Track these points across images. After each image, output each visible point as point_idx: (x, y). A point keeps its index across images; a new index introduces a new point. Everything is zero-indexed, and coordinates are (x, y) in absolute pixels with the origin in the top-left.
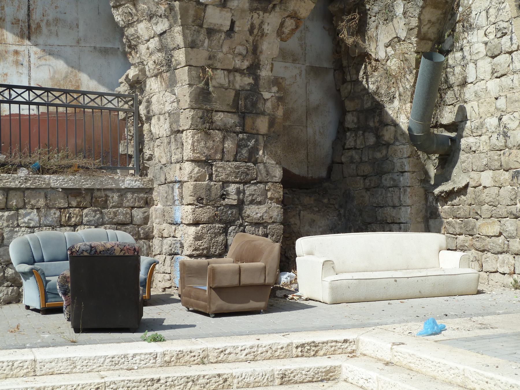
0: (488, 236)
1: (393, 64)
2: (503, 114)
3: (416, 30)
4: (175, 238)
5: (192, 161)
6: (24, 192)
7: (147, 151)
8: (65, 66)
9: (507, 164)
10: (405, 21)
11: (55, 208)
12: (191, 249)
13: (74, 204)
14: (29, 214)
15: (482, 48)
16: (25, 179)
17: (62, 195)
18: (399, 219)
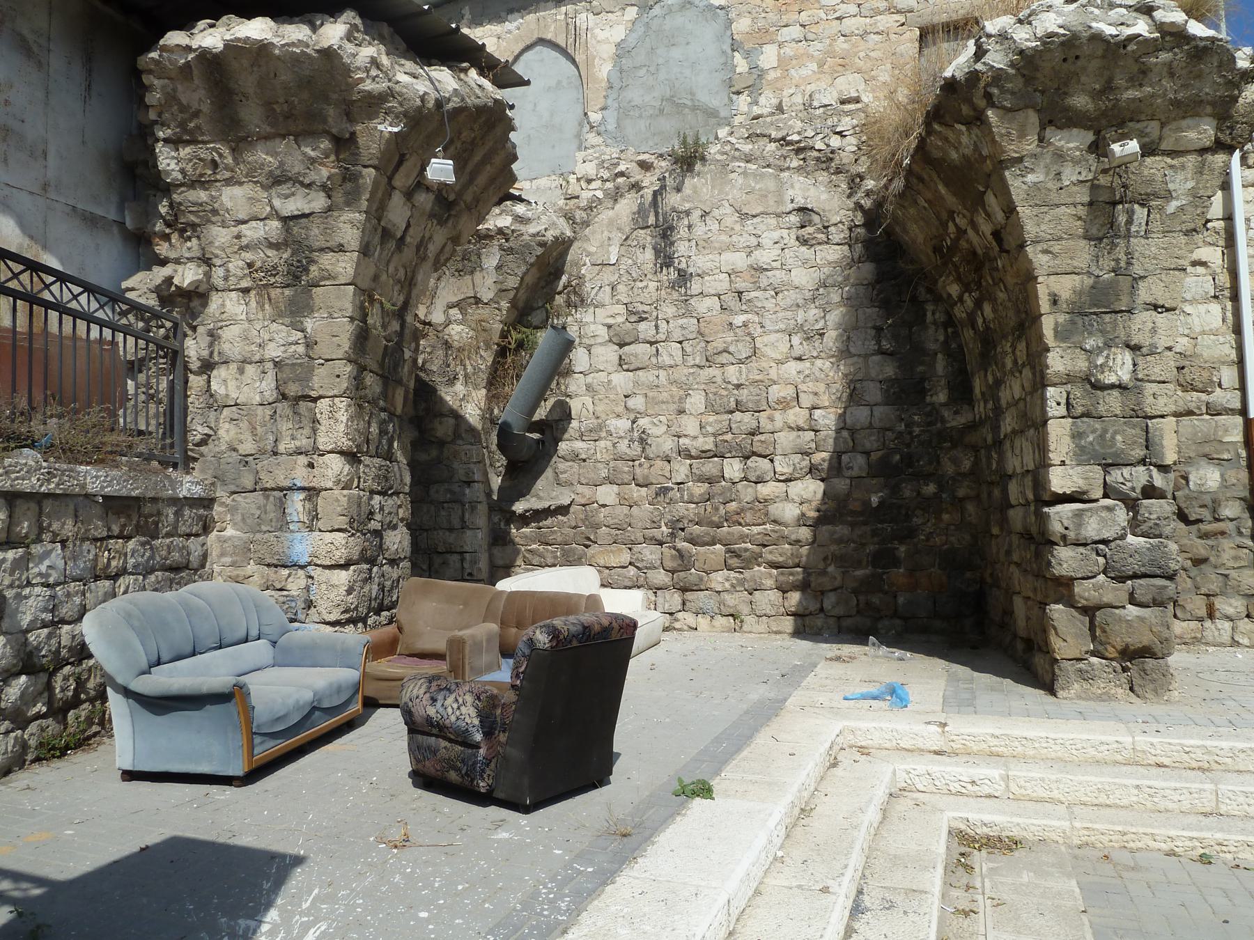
0: (607, 568)
1: (458, 332)
2: (638, 416)
4: (285, 593)
5: (342, 453)
6: (40, 504)
7: (200, 428)
8: (18, 231)
9: (646, 477)
11: (88, 539)
13: (116, 529)
14: (47, 554)
15: (603, 333)
16: (48, 473)
17: (97, 510)
18: (462, 547)
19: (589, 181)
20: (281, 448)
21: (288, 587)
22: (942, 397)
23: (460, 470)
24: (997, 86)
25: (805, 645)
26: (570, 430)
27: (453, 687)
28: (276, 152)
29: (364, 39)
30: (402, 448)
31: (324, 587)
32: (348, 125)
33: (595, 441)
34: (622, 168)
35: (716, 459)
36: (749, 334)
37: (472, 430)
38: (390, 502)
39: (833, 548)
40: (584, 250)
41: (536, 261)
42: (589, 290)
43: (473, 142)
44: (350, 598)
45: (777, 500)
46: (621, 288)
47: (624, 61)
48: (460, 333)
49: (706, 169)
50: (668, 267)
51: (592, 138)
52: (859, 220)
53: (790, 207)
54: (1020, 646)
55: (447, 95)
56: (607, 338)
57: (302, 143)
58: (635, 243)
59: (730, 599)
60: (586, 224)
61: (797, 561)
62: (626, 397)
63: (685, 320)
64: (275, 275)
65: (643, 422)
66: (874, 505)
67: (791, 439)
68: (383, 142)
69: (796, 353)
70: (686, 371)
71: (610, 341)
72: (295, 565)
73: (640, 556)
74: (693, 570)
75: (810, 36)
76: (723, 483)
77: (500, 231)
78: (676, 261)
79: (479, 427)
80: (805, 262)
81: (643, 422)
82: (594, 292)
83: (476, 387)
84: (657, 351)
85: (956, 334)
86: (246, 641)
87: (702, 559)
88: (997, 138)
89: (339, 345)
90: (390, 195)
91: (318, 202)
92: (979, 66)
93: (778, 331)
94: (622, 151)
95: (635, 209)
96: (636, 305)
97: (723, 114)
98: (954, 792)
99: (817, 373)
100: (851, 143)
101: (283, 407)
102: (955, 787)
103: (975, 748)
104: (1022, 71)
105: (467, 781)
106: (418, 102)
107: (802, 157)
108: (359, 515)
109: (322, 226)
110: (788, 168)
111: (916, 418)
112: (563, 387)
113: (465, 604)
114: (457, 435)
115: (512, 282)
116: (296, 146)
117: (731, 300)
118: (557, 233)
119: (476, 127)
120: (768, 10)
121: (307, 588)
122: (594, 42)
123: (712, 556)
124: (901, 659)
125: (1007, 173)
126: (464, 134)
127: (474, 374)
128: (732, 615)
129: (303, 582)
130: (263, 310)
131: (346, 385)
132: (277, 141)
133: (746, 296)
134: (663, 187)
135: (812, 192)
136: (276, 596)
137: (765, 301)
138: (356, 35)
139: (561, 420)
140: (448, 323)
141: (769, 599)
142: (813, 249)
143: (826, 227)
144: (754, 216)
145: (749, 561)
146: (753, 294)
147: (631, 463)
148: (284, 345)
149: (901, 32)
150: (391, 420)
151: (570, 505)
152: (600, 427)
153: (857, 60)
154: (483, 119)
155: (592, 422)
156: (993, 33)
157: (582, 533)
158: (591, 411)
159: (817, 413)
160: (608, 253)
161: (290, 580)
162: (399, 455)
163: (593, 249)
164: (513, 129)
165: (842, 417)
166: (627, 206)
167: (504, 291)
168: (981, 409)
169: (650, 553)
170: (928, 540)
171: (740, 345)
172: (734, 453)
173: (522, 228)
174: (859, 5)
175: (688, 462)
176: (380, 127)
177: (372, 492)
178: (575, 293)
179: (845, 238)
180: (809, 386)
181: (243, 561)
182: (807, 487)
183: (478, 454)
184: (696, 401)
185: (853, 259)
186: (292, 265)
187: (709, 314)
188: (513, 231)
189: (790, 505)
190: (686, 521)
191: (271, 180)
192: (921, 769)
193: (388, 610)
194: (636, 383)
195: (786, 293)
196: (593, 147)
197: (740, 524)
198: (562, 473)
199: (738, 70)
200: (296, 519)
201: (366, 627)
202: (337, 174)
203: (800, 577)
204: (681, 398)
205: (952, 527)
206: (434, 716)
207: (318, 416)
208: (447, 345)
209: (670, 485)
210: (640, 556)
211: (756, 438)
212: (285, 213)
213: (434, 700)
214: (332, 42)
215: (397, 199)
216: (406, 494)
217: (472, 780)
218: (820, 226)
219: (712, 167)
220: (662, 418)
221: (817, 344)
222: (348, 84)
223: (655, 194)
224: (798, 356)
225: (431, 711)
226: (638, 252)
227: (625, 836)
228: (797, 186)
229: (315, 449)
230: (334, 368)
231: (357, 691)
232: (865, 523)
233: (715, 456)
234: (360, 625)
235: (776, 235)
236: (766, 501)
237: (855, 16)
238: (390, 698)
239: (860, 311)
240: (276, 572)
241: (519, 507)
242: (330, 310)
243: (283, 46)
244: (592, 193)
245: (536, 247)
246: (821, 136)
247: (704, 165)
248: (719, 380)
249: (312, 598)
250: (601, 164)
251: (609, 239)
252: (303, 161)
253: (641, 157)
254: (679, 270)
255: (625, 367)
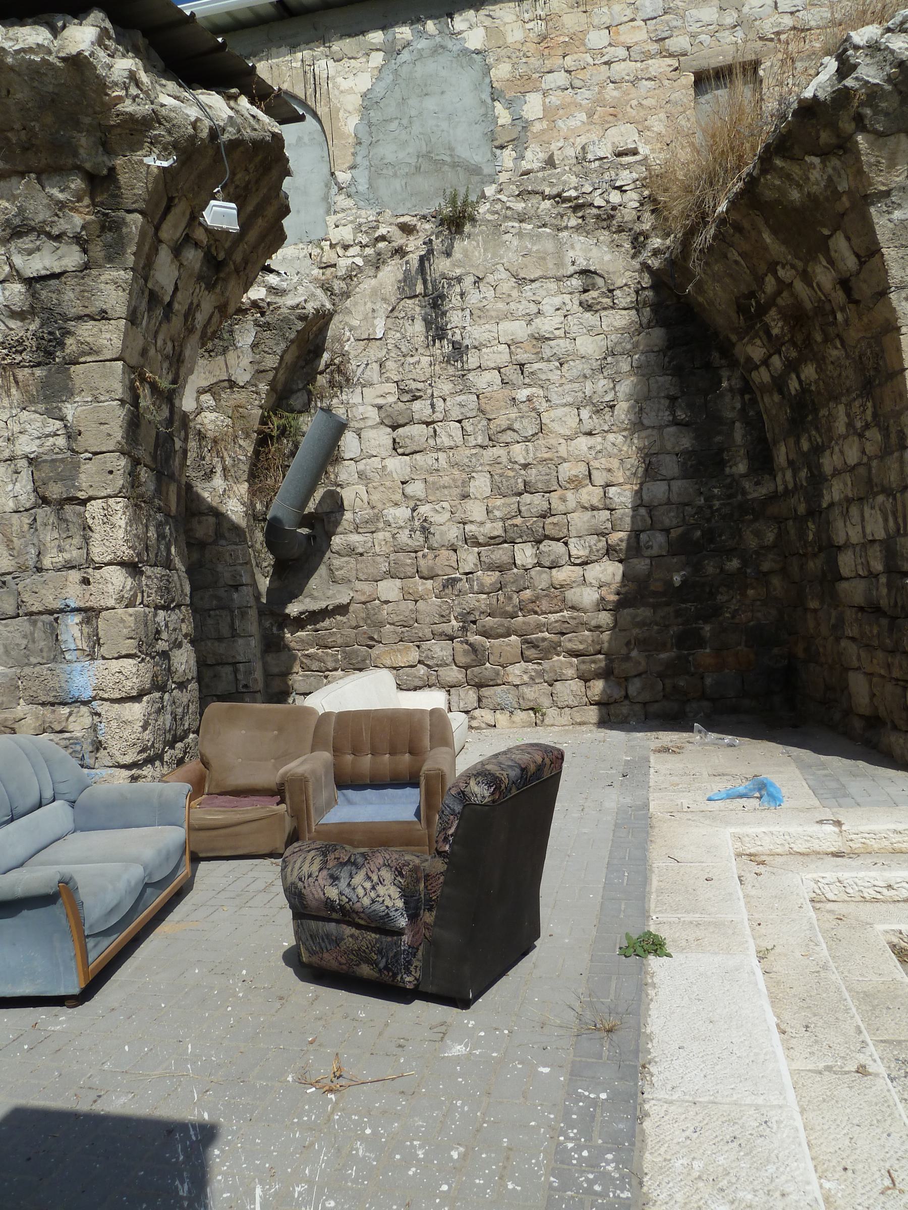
2: (418, 503)
3: (271, 375)
4: (67, 735)
5: (122, 564)
9: (431, 569)
10: (254, 357)
12: (134, 750)
15: (373, 415)
19: (346, 247)
20: (47, 562)
21: (70, 728)
22: (742, 468)
23: (226, 576)
24: (871, 106)
25: (616, 736)
26: (344, 523)
27: (360, 860)
28: (13, 195)
29: (116, 49)
30: (179, 553)
31: (114, 724)
32: (105, 159)
33: (372, 532)
34: (382, 231)
35: (506, 545)
36: (534, 409)
37: (235, 528)
38: (174, 617)
39: (636, 631)
40: (346, 323)
41: (297, 336)
42: (355, 368)
43: (246, 187)
44: (147, 735)
45: (574, 585)
46: (390, 364)
47: (372, 113)
48: (215, 421)
49: (477, 230)
50: (441, 339)
51: (342, 201)
52: (646, 281)
53: (571, 269)
54: (858, 724)
55: (222, 124)
56: (378, 420)
57: (46, 183)
58: (403, 314)
59: (530, 693)
60: (346, 295)
61: (598, 647)
62: (403, 483)
63: (463, 397)
64: (21, 352)
65: (424, 509)
66: (677, 585)
67: (585, 519)
68: (151, 179)
69: (587, 427)
70: (468, 452)
71: (382, 423)
72: (76, 702)
73: (430, 653)
74: (488, 665)
75: (577, 83)
76: (515, 570)
77: (255, 304)
78: (450, 333)
79: (243, 523)
80: (590, 330)
81: (424, 509)
82: (360, 369)
83: (237, 480)
84: (435, 431)
85: (754, 401)
86: (40, 805)
87: (496, 652)
88: (866, 169)
89: (109, 435)
90: (157, 250)
91: (72, 258)
92: (849, 82)
93: (565, 405)
94: (379, 214)
95: (400, 276)
96: (408, 382)
97: (487, 170)
98: (868, 898)
99: (610, 448)
100: (632, 199)
101: (44, 513)
102: (869, 893)
103: (876, 846)
104: (900, 87)
105: (386, 977)
106: (191, 131)
107: (580, 214)
108: (147, 636)
109: (78, 288)
110: (566, 227)
111: (716, 491)
112: (332, 476)
113: (280, 729)
114: (219, 535)
115: (271, 362)
116: (38, 186)
117: (512, 373)
118: (317, 305)
119: (251, 167)
120: (529, 54)
121: (94, 728)
122: (336, 92)
123: (508, 648)
124: (731, 745)
125: (872, 210)
126: (239, 176)
127: (233, 466)
128: (532, 709)
129: (87, 721)
130: (9, 396)
131: (121, 482)
132: (14, 180)
133: (528, 369)
134: (430, 252)
135: (595, 252)
136: (56, 740)
137: (549, 374)
138: (107, 42)
139: (332, 512)
140: (200, 410)
141: (569, 690)
142: (598, 315)
143: (611, 291)
144: (533, 281)
145: (547, 651)
146: (536, 366)
147: (413, 555)
148: (39, 438)
149: (674, 78)
150: (167, 523)
151: (349, 604)
152: (377, 518)
153: (629, 109)
154: (260, 157)
155: (367, 513)
156: (861, 44)
157: (365, 633)
158: (366, 501)
159: (612, 491)
160: (374, 326)
161: (71, 719)
162: (178, 563)
163: (356, 323)
164: (288, 173)
165: (638, 493)
166: (391, 273)
167: (262, 372)
168: (785, 478)
169: (440, 650)
170: (733, 617)
171: (525, 422)
172: (525, 538)
173: (280, 301)
174: (628, 48)
175: (476, 549)
176: (149, 161)
177: (157, 608)
178: (339, 371)
179: (632, 302)
180: (603, 462)
181: (10, 702)
182: (605, 570)
183: (243, 555)
184: (481, 484)
185: (641, 325)
186: (43, 338)
187: (490, 389)
188: (269, 304)
189: (588, 589)
190: (477, 613)
191: (8, 231)
192: (831, 876)
193: (181, 741)
194: (414, 468)
195: (571, 363)
196: (343, 210)
197: (536, 613)
198: (337, 570)
199: (501, 122)
200: (73, 647)
201: (163, 765)
202: (94, 221)
203: (603, 664)
204: (464, 482)
205: (758, 603)
206: (336, 898)
207: (90, 521)
208: (201, 436)
209: (458, 575)
210: (430, 653)
211: (549, 520)
212: (29, 273)
213: (334, 879)
214: (82, 47)
215: (164, 255)
216: (187, 605)
217: (395, 975)
218: (604, 290)
219: (483, 228)
220: (445, 504)
221: (607, 417)
222: (103, 104)
223: (422, 259)
224: (588, 431)
225: (332, 893)
226: (407, 325)
227: (610, 1031)
228: (578, 246)
229: (90, 561)
230: (105, 462)
231: (184, 853)
232: (668, 604)
233: (505, 542)
234: (157, 763)
235: (557, 301)
236: (562, 586)
237: (624, 60)
238: (213, 850)
239: (652, 380)
240: (54, 711)
241: (293, 609)
242: (95, 392)
243: (18, 52)
244: (350, 261)
245: (296, 321)
246: (599, 191)
247: (474, 226)
248: (504, 460)
249: (101, 738)
250: (358, 228)
251: (374, 311)
252: (48, 206)
253: (401, 220)
254: (453, 343)
255: (400, 451)
